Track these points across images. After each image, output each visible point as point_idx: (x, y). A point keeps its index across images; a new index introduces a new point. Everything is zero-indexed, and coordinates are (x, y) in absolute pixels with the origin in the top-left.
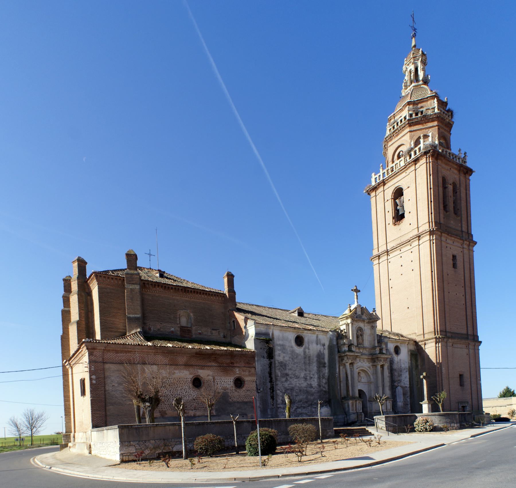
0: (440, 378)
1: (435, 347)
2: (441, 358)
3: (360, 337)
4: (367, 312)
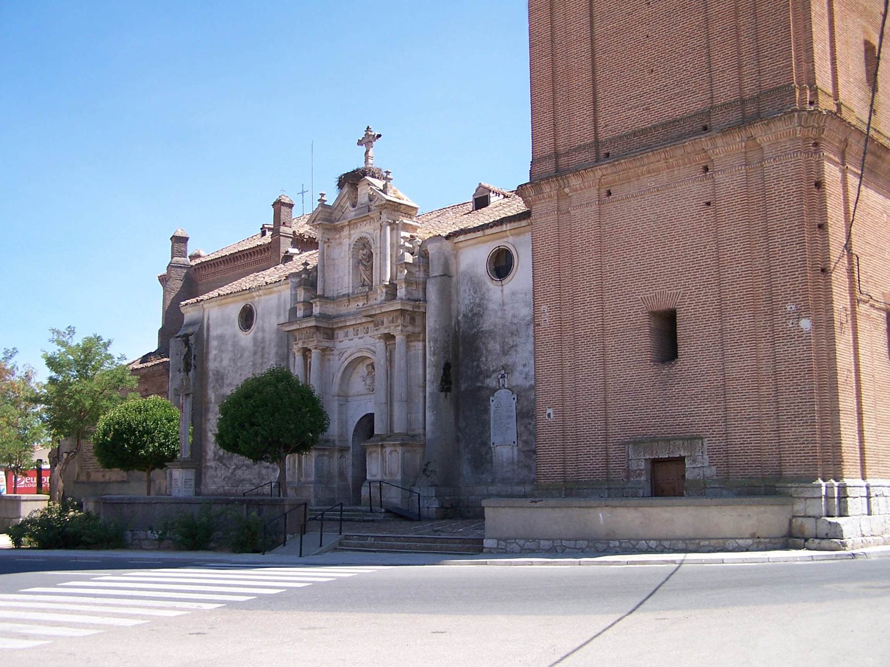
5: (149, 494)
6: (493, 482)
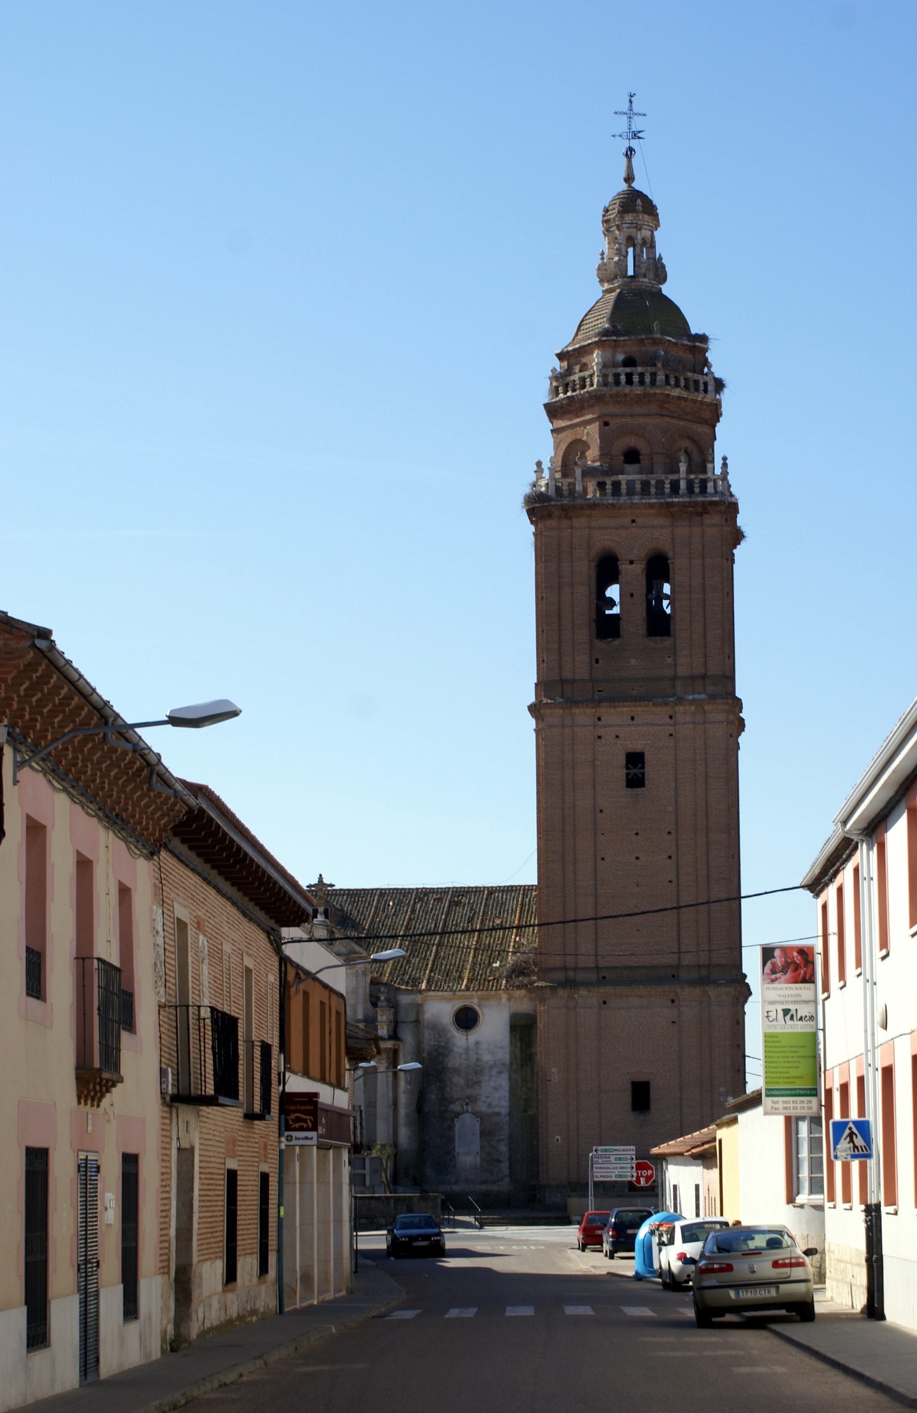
5: (698, 1215)
6: (456, 1183)
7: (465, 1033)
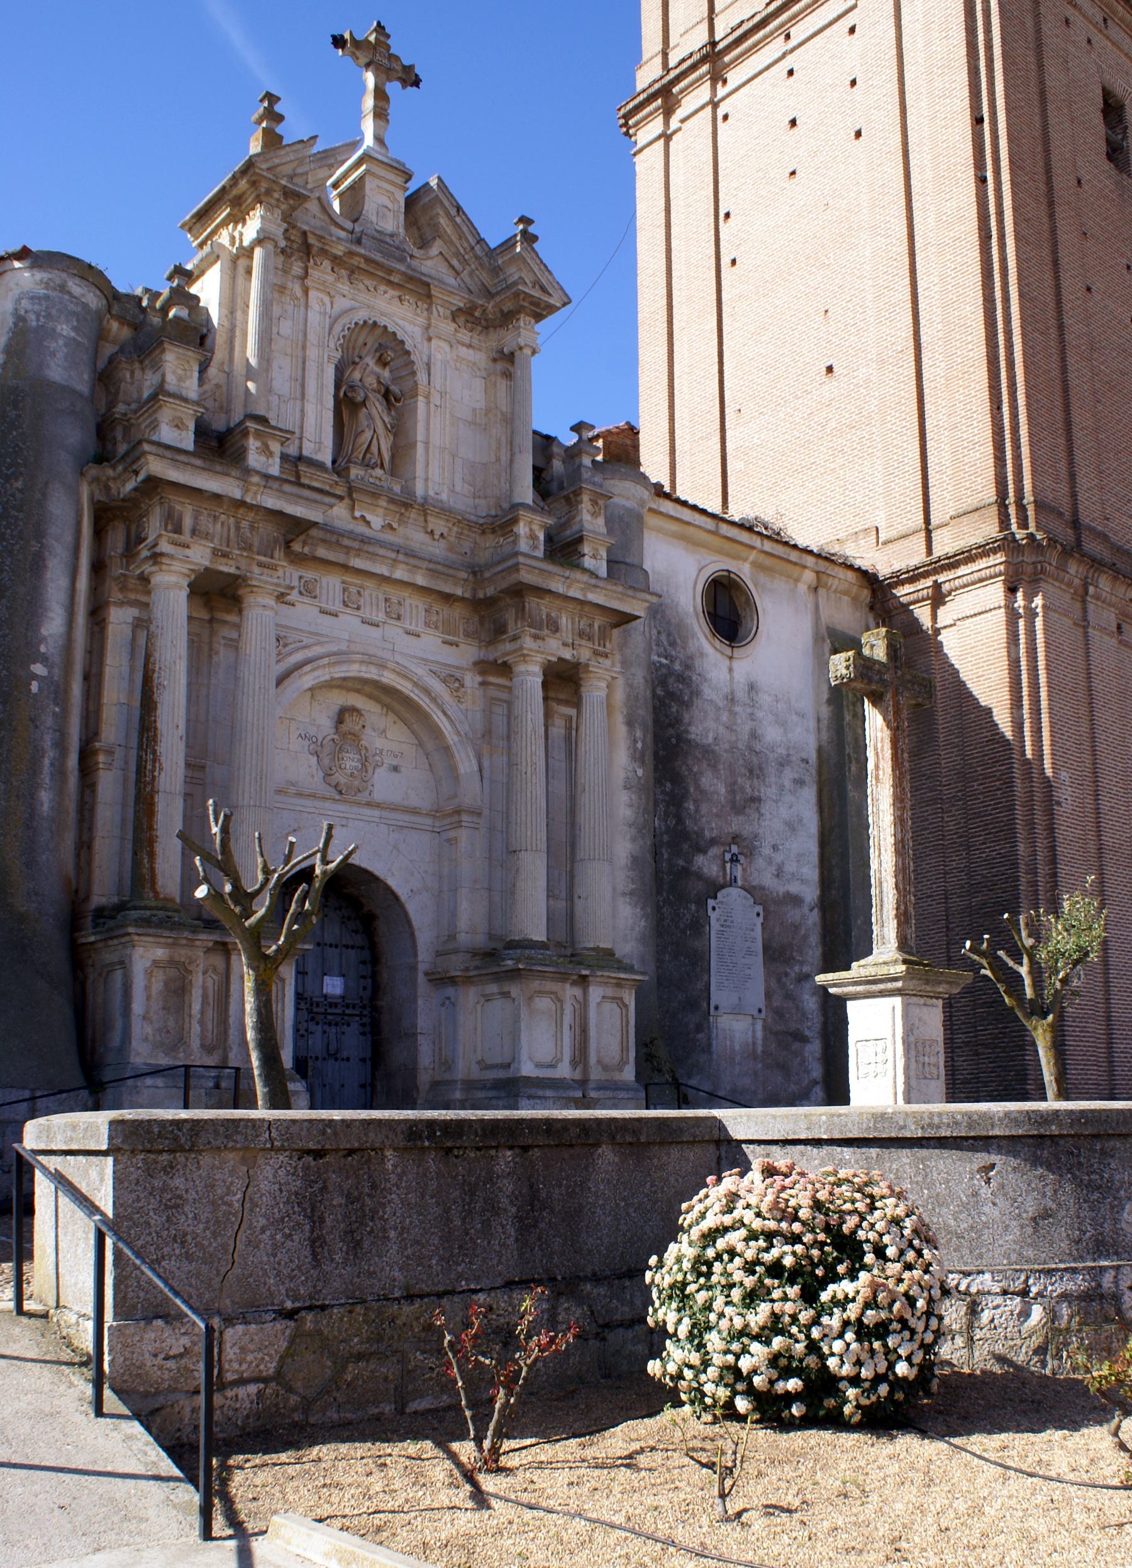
0: (1041, 844)
1: (1001, 615)
2: (1025, 450)
3: (376, 407)
4: (461, 236)
7: (728, 651)
